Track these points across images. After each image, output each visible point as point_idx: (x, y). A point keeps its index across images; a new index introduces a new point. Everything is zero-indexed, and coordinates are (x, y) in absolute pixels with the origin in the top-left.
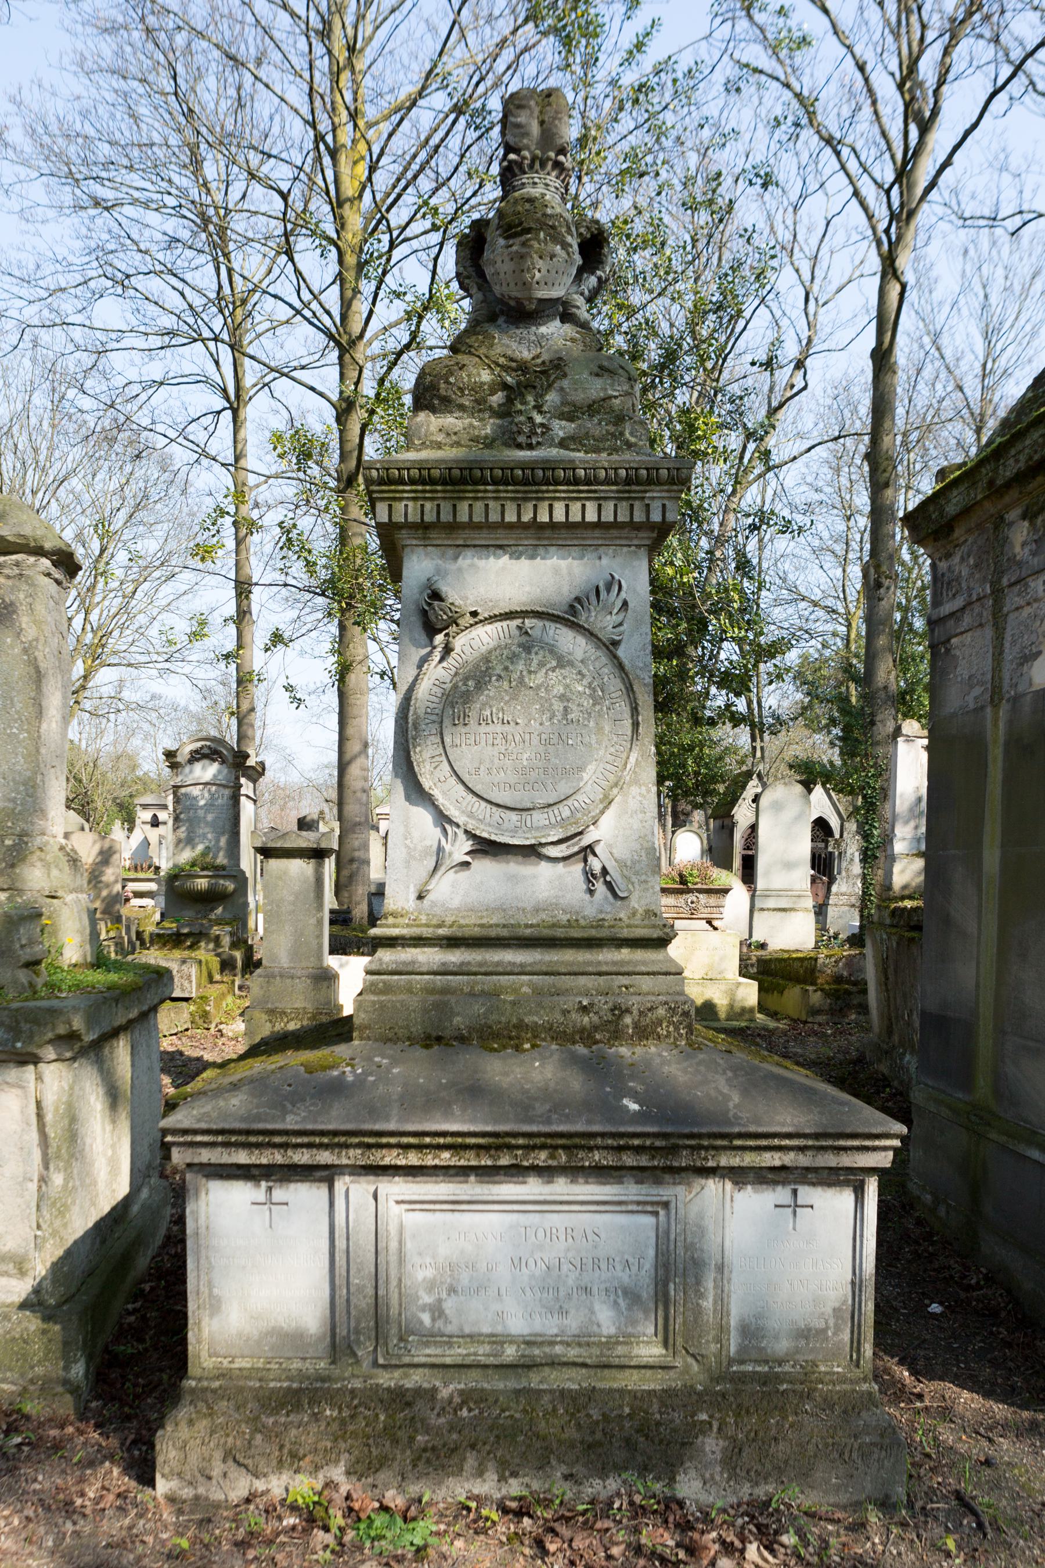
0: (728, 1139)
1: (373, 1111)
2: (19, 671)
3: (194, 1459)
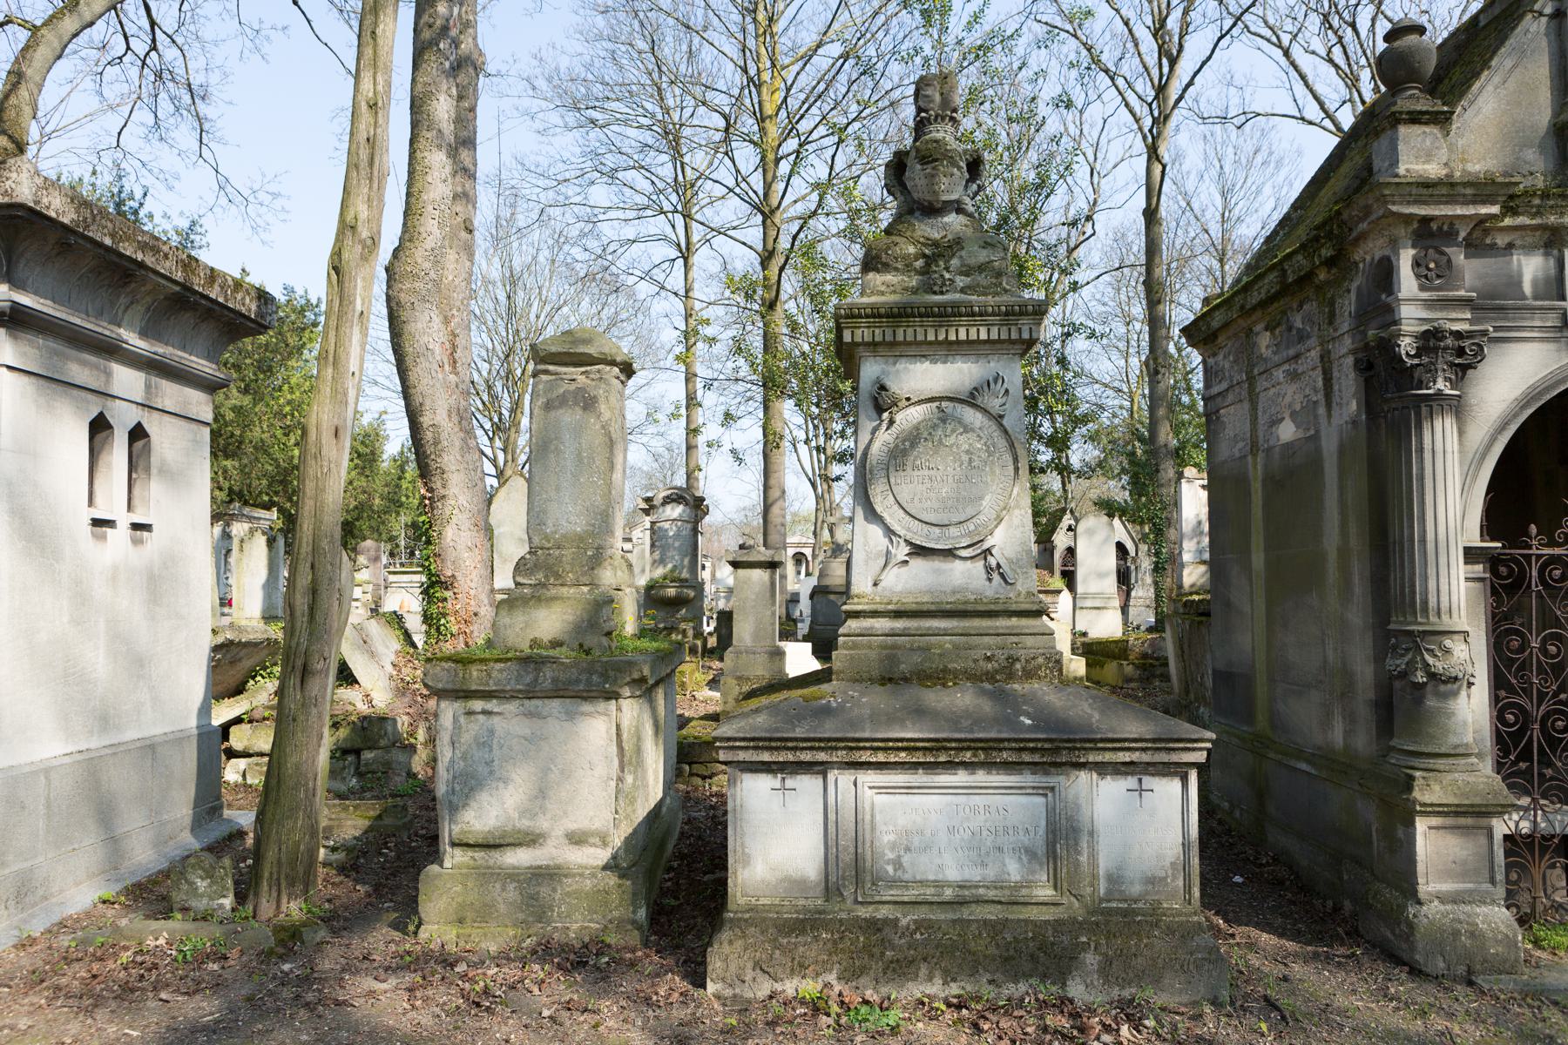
0: (1094, 743)
1: (853, 724)
2: (599, 440)
3: (733, 968)
